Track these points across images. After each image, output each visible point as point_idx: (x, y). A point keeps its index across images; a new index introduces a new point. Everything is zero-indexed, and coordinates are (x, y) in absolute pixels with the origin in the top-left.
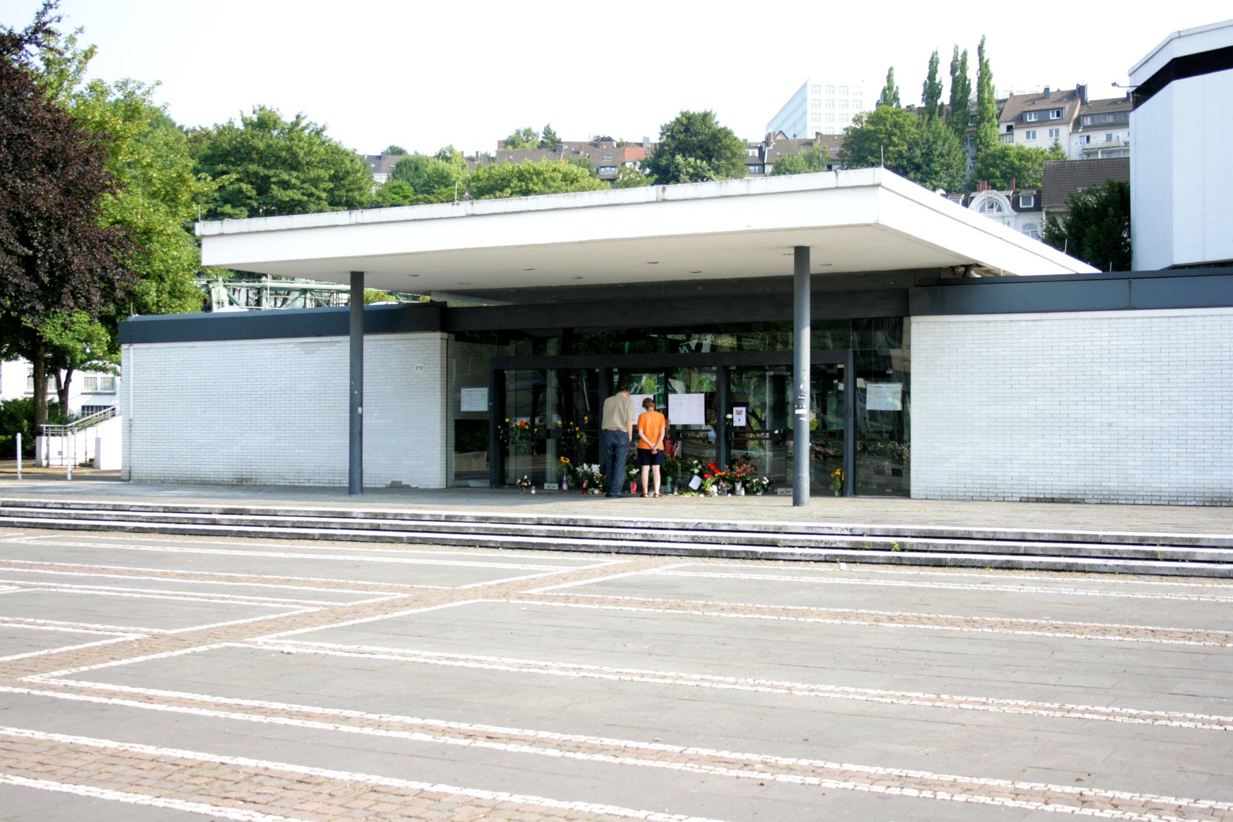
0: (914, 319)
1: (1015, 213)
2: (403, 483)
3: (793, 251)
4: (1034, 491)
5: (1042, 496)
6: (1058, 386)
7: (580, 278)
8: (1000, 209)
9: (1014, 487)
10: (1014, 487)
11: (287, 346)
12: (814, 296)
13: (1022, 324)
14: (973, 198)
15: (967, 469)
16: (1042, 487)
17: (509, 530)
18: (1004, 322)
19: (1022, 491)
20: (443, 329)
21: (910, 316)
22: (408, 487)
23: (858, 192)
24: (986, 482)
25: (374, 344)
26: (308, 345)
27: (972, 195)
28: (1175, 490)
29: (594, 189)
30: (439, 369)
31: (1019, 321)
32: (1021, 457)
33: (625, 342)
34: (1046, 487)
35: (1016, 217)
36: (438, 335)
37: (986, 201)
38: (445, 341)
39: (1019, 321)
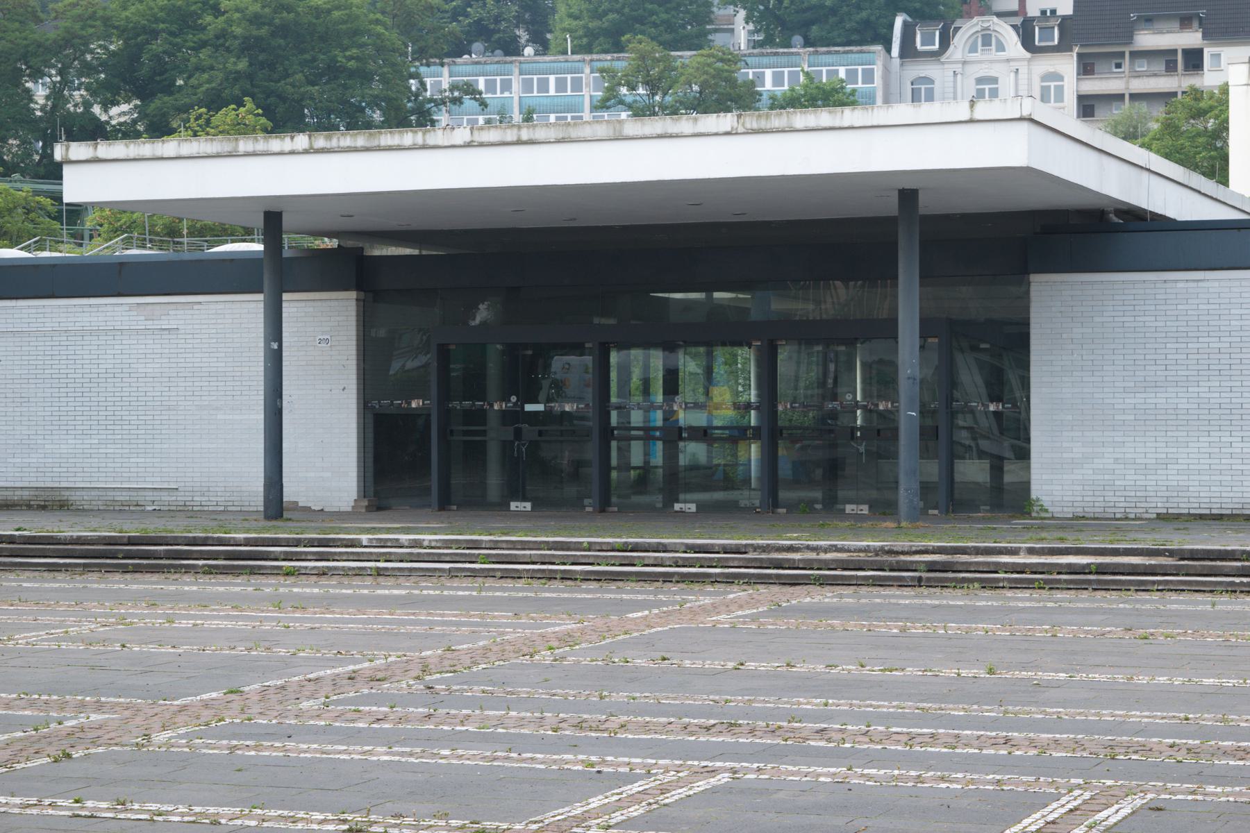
0: (1035, 278)
1: (1028, 55)
2: (300, 504)
3: (897, 192)
4: (1219, 506)
5: (1207, 512)
6: (1228, 367)
7: (575, 219)
8: (1001, 47)
9: (1171, 500)
10: (1171, 500)
11: (116, 309)
12: (926, 247)
13: (1180, 285)
14: (957, 29)
15: (1107, 477)
16: (1208, 500)
17: (371, 553)
18: (1155, 282)
19: (1181, 505)
20: (358, 288)
21: (1029, 274)
22: (307, 509)
23: (997, 125)
24: (1133, 494)
25: (295, 306)
26: (150, 307)
27: (956, 24)
28: (1101, 510)
29: (654, 114)
30: (354, 343)
31: (1176, 281)
32: (1180, 461)
33: (265, 242)
34: (1213, 500)
35: (1029, 60)
36: (353, 295)
37: (979, 35)
38: (362, 303)
39: (1176, 281)
